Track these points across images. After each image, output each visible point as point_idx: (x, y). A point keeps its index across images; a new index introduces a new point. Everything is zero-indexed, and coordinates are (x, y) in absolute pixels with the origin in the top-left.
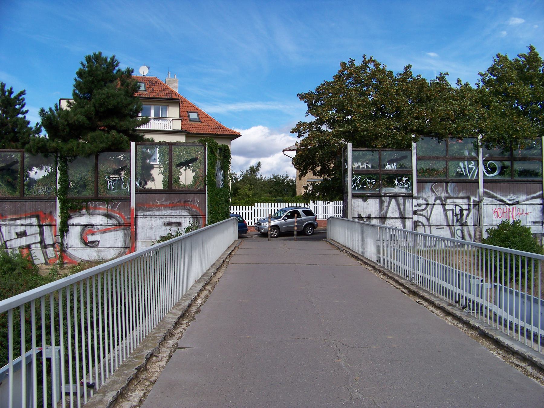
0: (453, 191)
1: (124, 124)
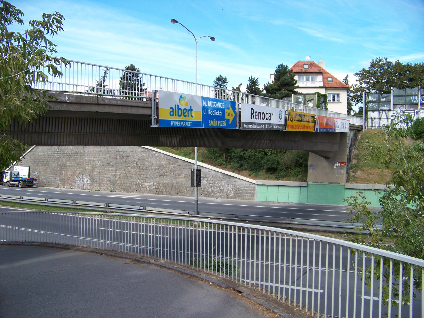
0: (408, 108)
1: (290, 88)
